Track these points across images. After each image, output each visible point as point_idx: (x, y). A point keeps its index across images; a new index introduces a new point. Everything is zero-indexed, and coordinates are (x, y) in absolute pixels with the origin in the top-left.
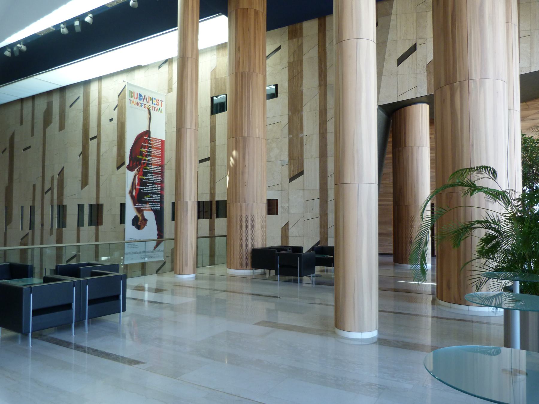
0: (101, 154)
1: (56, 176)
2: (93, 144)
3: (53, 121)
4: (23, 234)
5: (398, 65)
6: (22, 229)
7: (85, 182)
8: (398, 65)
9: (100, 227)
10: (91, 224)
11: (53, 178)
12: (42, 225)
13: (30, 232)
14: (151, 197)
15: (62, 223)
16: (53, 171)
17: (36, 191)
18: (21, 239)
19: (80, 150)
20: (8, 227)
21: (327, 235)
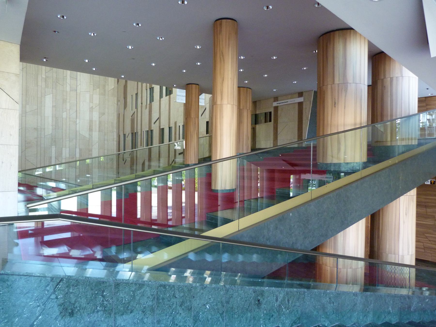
10: (166, 95)
12: (142, 104)
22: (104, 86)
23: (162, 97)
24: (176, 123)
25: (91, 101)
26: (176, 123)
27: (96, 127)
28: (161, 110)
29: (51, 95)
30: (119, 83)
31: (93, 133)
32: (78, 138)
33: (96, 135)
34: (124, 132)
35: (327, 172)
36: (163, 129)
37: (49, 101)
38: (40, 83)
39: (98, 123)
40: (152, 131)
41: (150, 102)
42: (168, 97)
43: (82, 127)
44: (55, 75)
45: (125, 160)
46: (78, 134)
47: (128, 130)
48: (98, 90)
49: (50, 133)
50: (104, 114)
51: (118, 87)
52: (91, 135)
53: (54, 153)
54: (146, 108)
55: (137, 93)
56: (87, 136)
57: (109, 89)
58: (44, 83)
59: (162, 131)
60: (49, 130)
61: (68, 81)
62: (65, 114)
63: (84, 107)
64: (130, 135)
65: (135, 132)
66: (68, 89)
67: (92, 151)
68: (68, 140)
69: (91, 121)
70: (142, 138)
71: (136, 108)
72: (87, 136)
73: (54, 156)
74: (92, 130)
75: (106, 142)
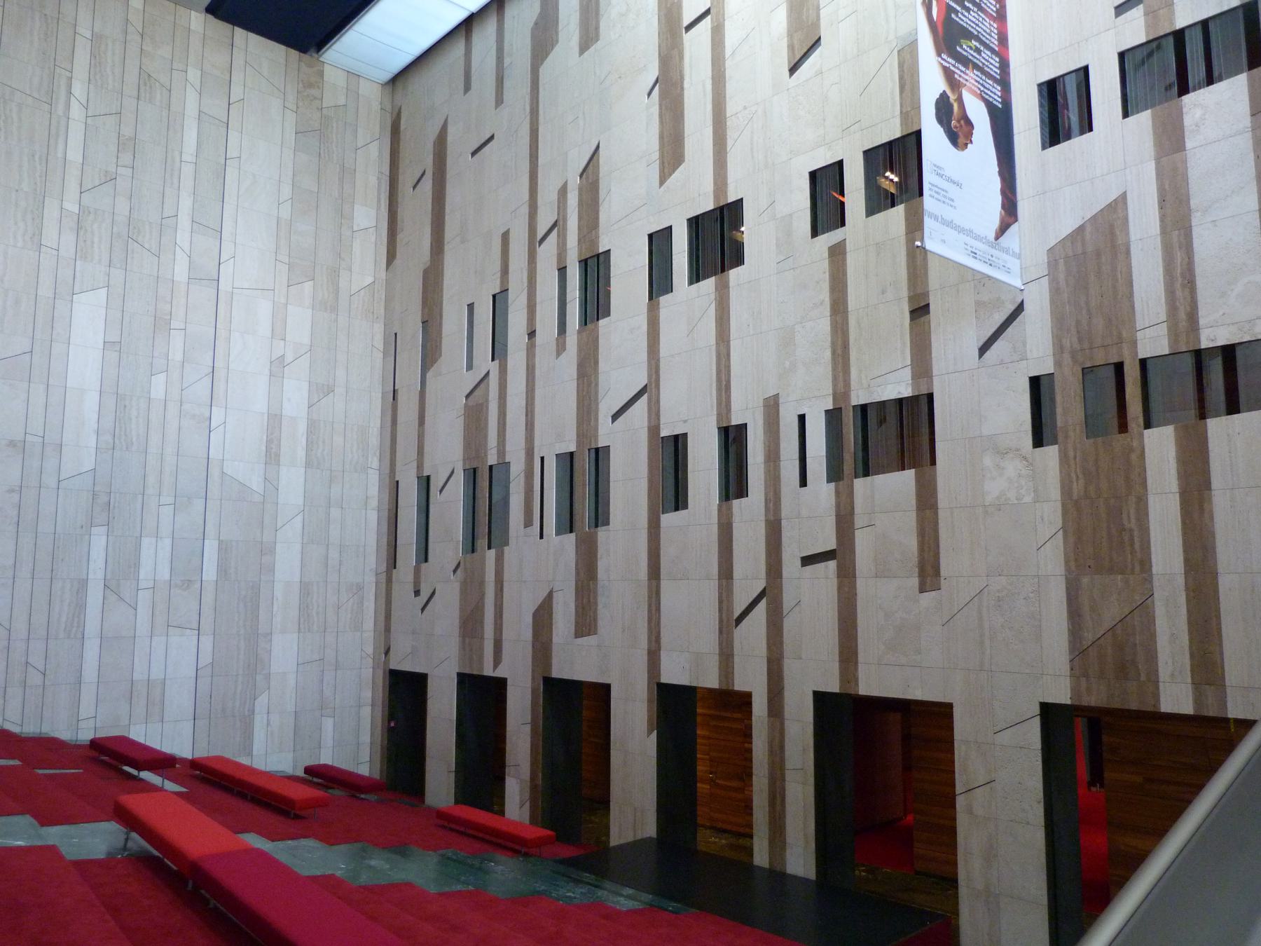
0: (728, 52)
1: (574, 182)
2: (697, 44)
3: (562, 36)
4: (471, 379)
5: (1124, 197)
6: (470, 367)
7: (672, 153)
8: (1124, 197)
9: (734, 274)
10: (696, 276)
11: (563, 192)
12: (532, 334)
13: (494, 367)
14: (978, 51)
15: (596, 303)
16: (563, 167)
17: (398, 454)
18: (467, 397)
19: (653, 72)
20: (429, 375)
21: (1146, 487)
22: (334, 274)
23: (668, 288)
24: (772, 407)
25: (278, 331)
26: (772, 407)
27: (294, 446)
28: (664, 351)
29: (103, 292)
30: (397, 262)
31: (284, 471)
32: (214, 490)
33: (292, 483)
34: (420, 466)
35: (654, 583)
36: (428, 477)
37: (88, 318)
38: (50, 233)
39: (302, 427)
40: (600, 456)
41: (585, 321)
42: (709, 284)
43: (236, 445)
44: (122, 206)
45: (425, 595)
46: (215, 472)
47: (446, 454)
48: (308, 286)
49: (88, 464)
50: (330, 390)
51: (388, 282)
52: (271, 484)
53: (101, 563)
54: (561, 348)
55: (505, 291)
56: (256, 483)
57: (355, 289)
58: (69, 238)
59: (673, 451)
60: (82, 452)
61: (183, 238)
62: (159, 382)
63: (247, 353)
64: (460, 477)
65: (492, 460)
66: (181, 272)
67: (272, 551)
68: (171, 500)
69: (274, 421)
70: (530, 496)
71: (498, 350)
72: (256, 483)
73: (100, 575)
74: (278, 455)
75: (335, 513)
